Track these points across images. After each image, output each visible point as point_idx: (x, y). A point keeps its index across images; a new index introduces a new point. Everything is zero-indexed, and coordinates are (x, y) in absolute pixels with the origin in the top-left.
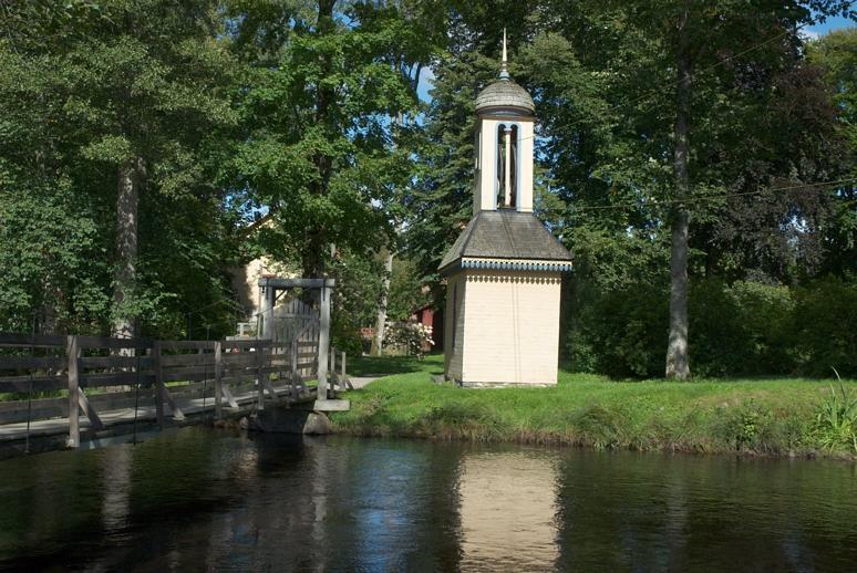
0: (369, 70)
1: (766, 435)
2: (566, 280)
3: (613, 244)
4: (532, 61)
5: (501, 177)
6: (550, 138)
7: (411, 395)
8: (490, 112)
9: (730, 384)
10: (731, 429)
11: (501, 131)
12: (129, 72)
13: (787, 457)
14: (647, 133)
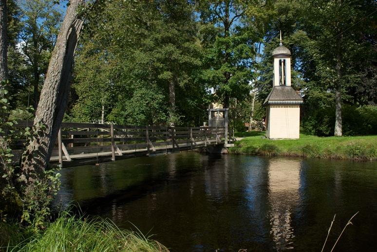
0: (240, 46)
1: (363, 154)
2: (301, 106)
3: (322, 95)
4: (294, 39)
5: (281, 75)
6: (302, 63)
7: (256, 142)
8: (277, 56)
9: (353, 137)
10: (351, 152)
11: (280, 61)
12: (171, 53)
13: (370, 160)
14: (328, 59)
